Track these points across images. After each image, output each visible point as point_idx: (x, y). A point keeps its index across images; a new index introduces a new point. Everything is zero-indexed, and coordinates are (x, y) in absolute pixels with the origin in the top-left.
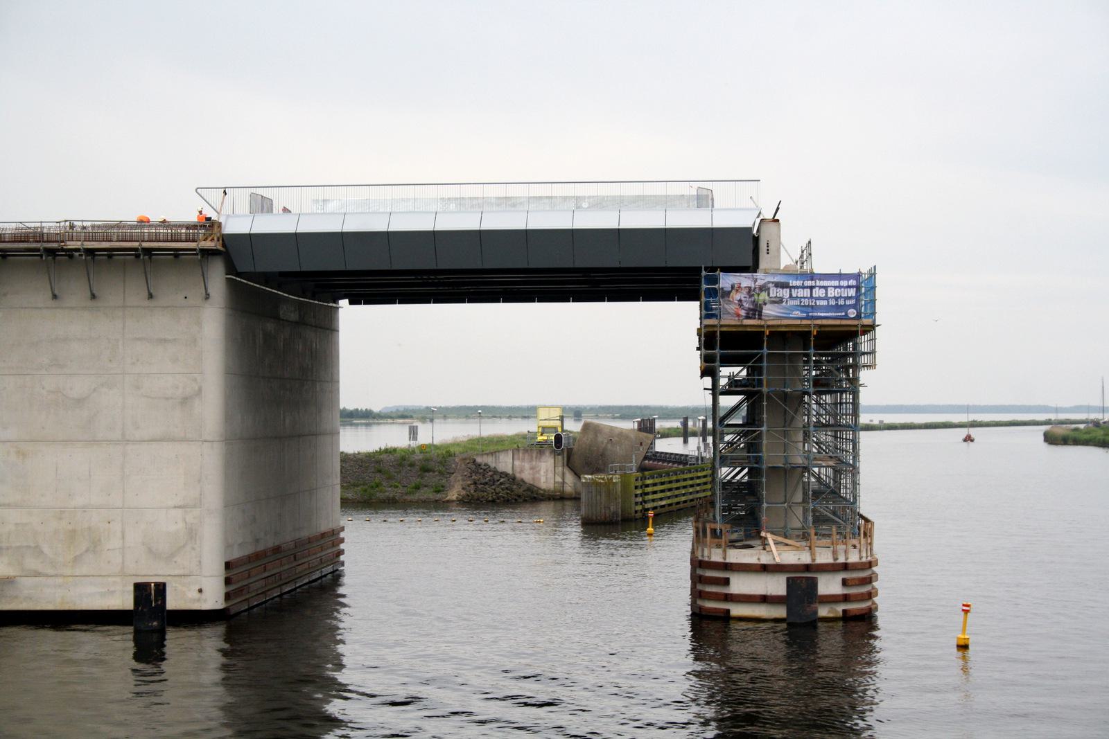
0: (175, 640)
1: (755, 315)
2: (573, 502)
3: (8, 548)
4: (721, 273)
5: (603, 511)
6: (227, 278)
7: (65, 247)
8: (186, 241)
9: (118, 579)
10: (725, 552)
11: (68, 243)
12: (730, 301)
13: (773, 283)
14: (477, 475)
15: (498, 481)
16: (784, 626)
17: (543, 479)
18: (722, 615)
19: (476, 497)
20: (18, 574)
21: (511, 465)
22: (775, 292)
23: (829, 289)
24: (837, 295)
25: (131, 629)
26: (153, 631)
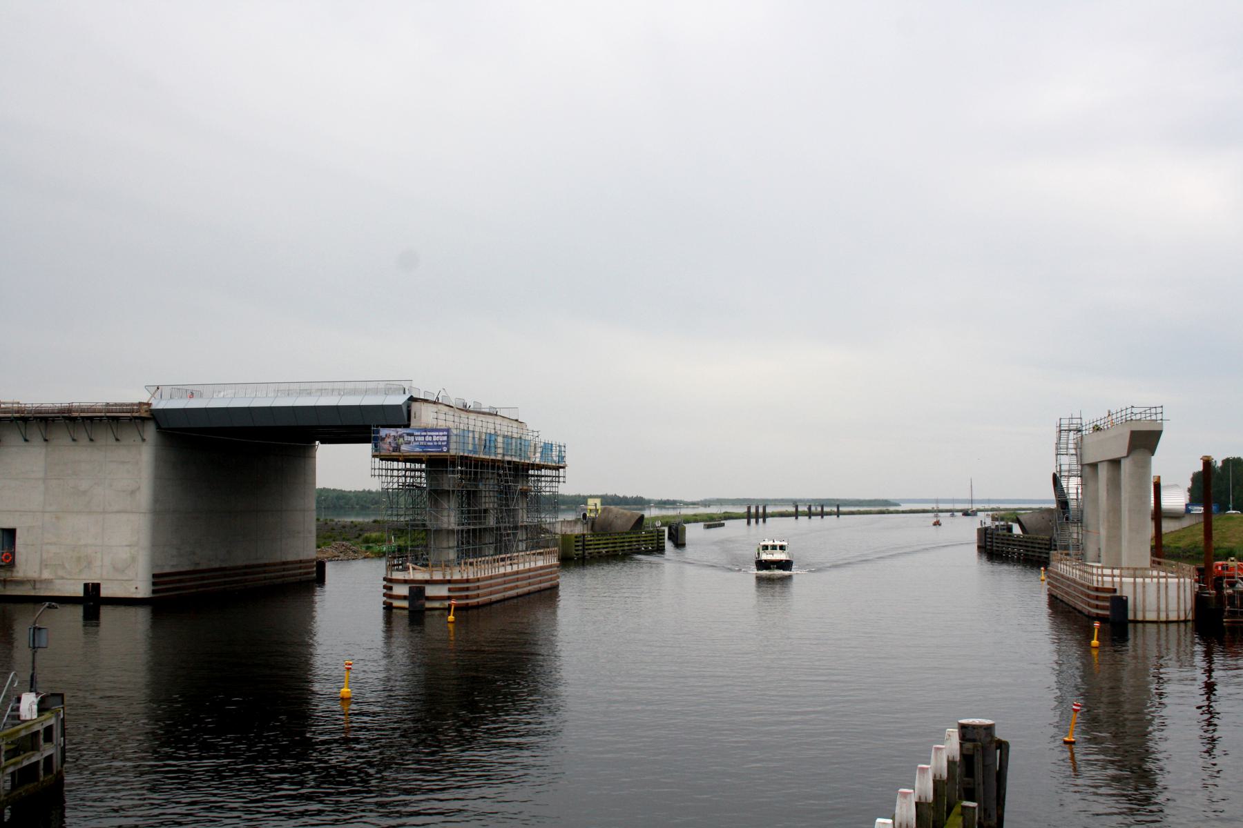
0: (106, 613)
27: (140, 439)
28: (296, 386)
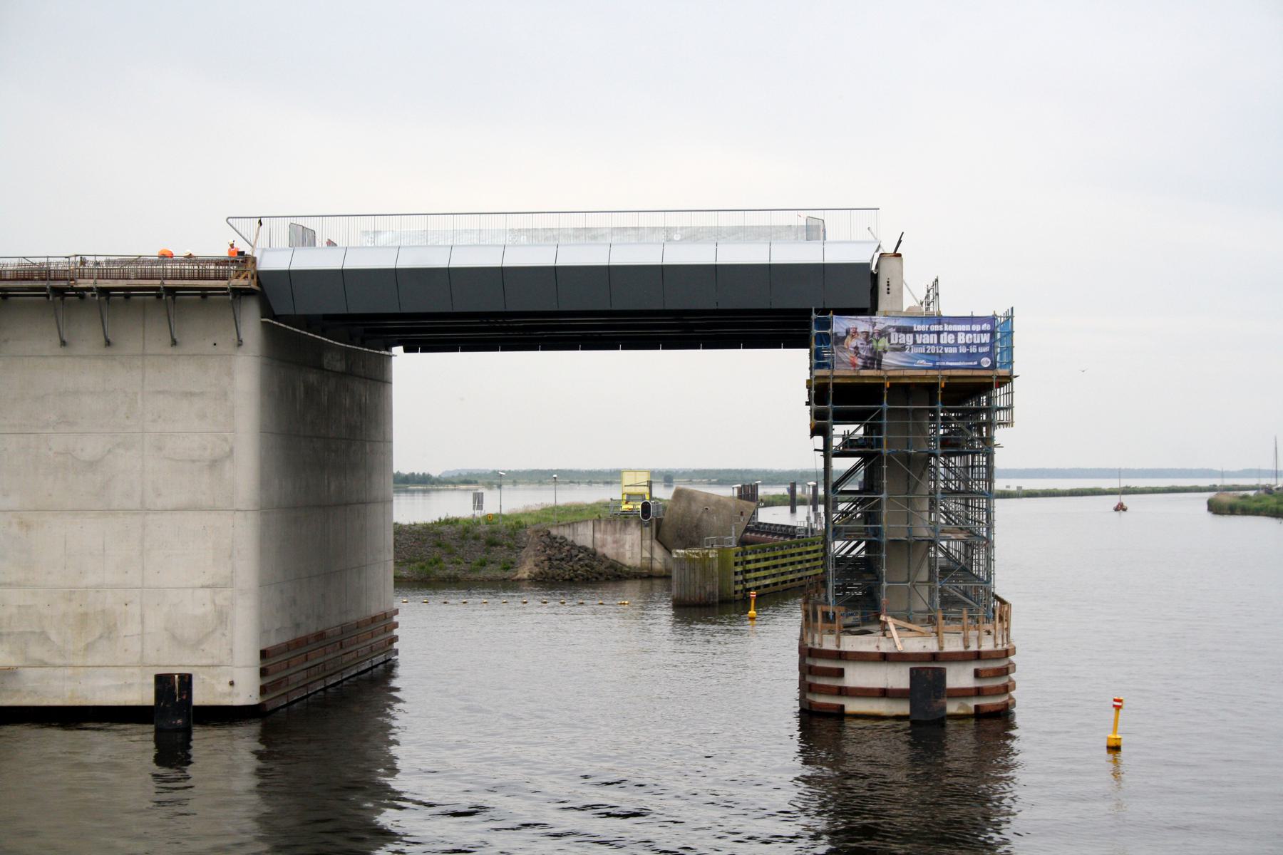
0: (203, 741)
1: (874, 364)
2: (664, 580)
3: (9, 634)
4: (834, 316)
5: (698, 591)
7: (75, 286)
8: (215, 279)
9: (136, 670)
10: (838, 638)
11: (79, 281)
12: (844, 348)
13: (894, 327)
14: (553, 549)
15: (576, 556)
17: (628, 554)
18: (835, 711)
19: (550, 575)
21: (591, 539)
22: (896, 338)
23: (959, 334)
24: (968, 342)
25: (151, 728)
26: (177, 730)
27: (169, 339)
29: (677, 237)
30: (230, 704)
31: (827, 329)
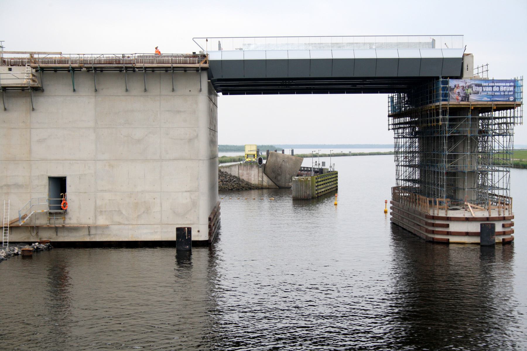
1: (466, 99)
2: (267, 190)
3: (105, 211)
4: (450, 80)
5: (304, 194)
6: (208, 82)
7: (135, 66)
8: (190, 63)
9: (159, 226)
10: (446, 211)
11: (137, 64)
12: (454, 93)
13: (474, 84)
14: (223, 177)
15: (233, 180)
16: (479, 246)
17: (253, 179)
18: (446, 242)
19: (223, 188)
20: (110, 224)
21: (237, 173)
22: (475, 89)
23: (501, 87)
24: (504, 90)
26: (187, 251)
27: (72, 89)
28: (328, 40)
29: (374, 47)
30: (198, 240)
31: (447, 85)
